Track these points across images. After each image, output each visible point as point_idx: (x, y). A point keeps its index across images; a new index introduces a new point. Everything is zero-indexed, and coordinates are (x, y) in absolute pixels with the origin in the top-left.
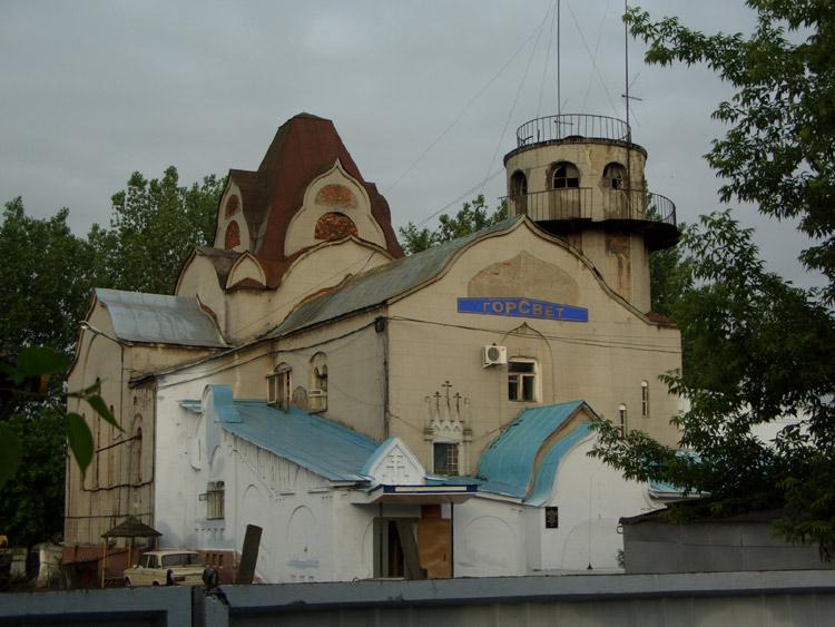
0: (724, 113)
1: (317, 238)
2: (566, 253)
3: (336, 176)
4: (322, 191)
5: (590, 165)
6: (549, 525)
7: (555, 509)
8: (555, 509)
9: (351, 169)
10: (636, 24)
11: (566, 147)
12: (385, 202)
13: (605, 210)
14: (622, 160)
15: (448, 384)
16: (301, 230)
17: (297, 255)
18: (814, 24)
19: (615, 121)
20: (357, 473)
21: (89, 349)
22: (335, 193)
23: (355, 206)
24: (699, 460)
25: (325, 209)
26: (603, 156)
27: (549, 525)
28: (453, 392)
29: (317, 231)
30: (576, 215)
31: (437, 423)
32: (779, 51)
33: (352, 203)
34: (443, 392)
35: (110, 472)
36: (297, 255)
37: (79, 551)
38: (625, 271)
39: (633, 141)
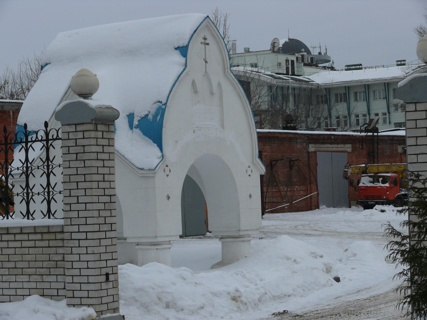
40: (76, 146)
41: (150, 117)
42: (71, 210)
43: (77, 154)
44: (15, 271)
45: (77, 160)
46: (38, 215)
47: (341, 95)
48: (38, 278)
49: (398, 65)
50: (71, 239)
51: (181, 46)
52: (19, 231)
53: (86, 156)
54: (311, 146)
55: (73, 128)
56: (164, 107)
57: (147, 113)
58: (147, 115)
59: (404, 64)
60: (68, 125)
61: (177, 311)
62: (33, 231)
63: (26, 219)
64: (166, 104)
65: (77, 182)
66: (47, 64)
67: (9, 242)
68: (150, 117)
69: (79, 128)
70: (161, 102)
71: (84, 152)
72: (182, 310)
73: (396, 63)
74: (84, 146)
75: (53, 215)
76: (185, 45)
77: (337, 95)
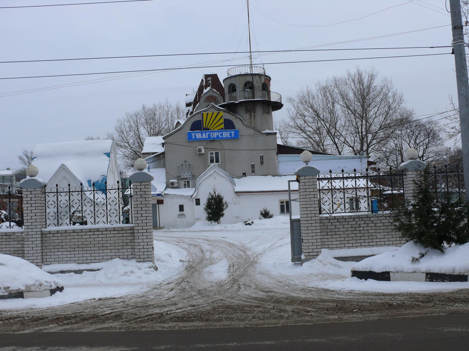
2: (229, 114)
4: (206, 98)
5: (258, 84)
6: (197, 204)
7: (199, 199)
8: (199, 199)
11: (232, 78)
14: (251, 80)
15: (185, 161)
18: (444, 241)
19: (261, 68)
21: (214, 126)
26: (243, 82)
27: (197, 204)
28: (187, 164)
31: (182, 173)
34: (184, 164)
37: (461, 29)
38: (253, 117)
39: (266, 74)
40: (141, 191)
41: (100, 182)
42: (138, 220)
43: (141, 195)
44: (102, 248)
45: (141, 198)
46: (113, 222)
47: (8, 179)
48: (117, 251)
49: (7, 170)
50: (138, 233)
51: (107, 152)
52: (105, 230)
53: (146, 196)
54: (4, 199)
55: (139, 184)
56: (106, 178)
57: (98, 180)
58: (98, 181)
59: (9, 170)
60: (136, 182)
61: (162, 262)
62: (113, 230)
63: (9, 229)
64: (107, 176)
65: (142, 208)
66: (35, 158)
67: (91, 236)
68: (100, 182)
69: (142, 184)
70: (104, 176)
71: (145, 194)
72: (164, 261)
73: (6, 169)
74: (145, 192)
75: (12, 227)
76: (109, 152)
77: (6, 179)
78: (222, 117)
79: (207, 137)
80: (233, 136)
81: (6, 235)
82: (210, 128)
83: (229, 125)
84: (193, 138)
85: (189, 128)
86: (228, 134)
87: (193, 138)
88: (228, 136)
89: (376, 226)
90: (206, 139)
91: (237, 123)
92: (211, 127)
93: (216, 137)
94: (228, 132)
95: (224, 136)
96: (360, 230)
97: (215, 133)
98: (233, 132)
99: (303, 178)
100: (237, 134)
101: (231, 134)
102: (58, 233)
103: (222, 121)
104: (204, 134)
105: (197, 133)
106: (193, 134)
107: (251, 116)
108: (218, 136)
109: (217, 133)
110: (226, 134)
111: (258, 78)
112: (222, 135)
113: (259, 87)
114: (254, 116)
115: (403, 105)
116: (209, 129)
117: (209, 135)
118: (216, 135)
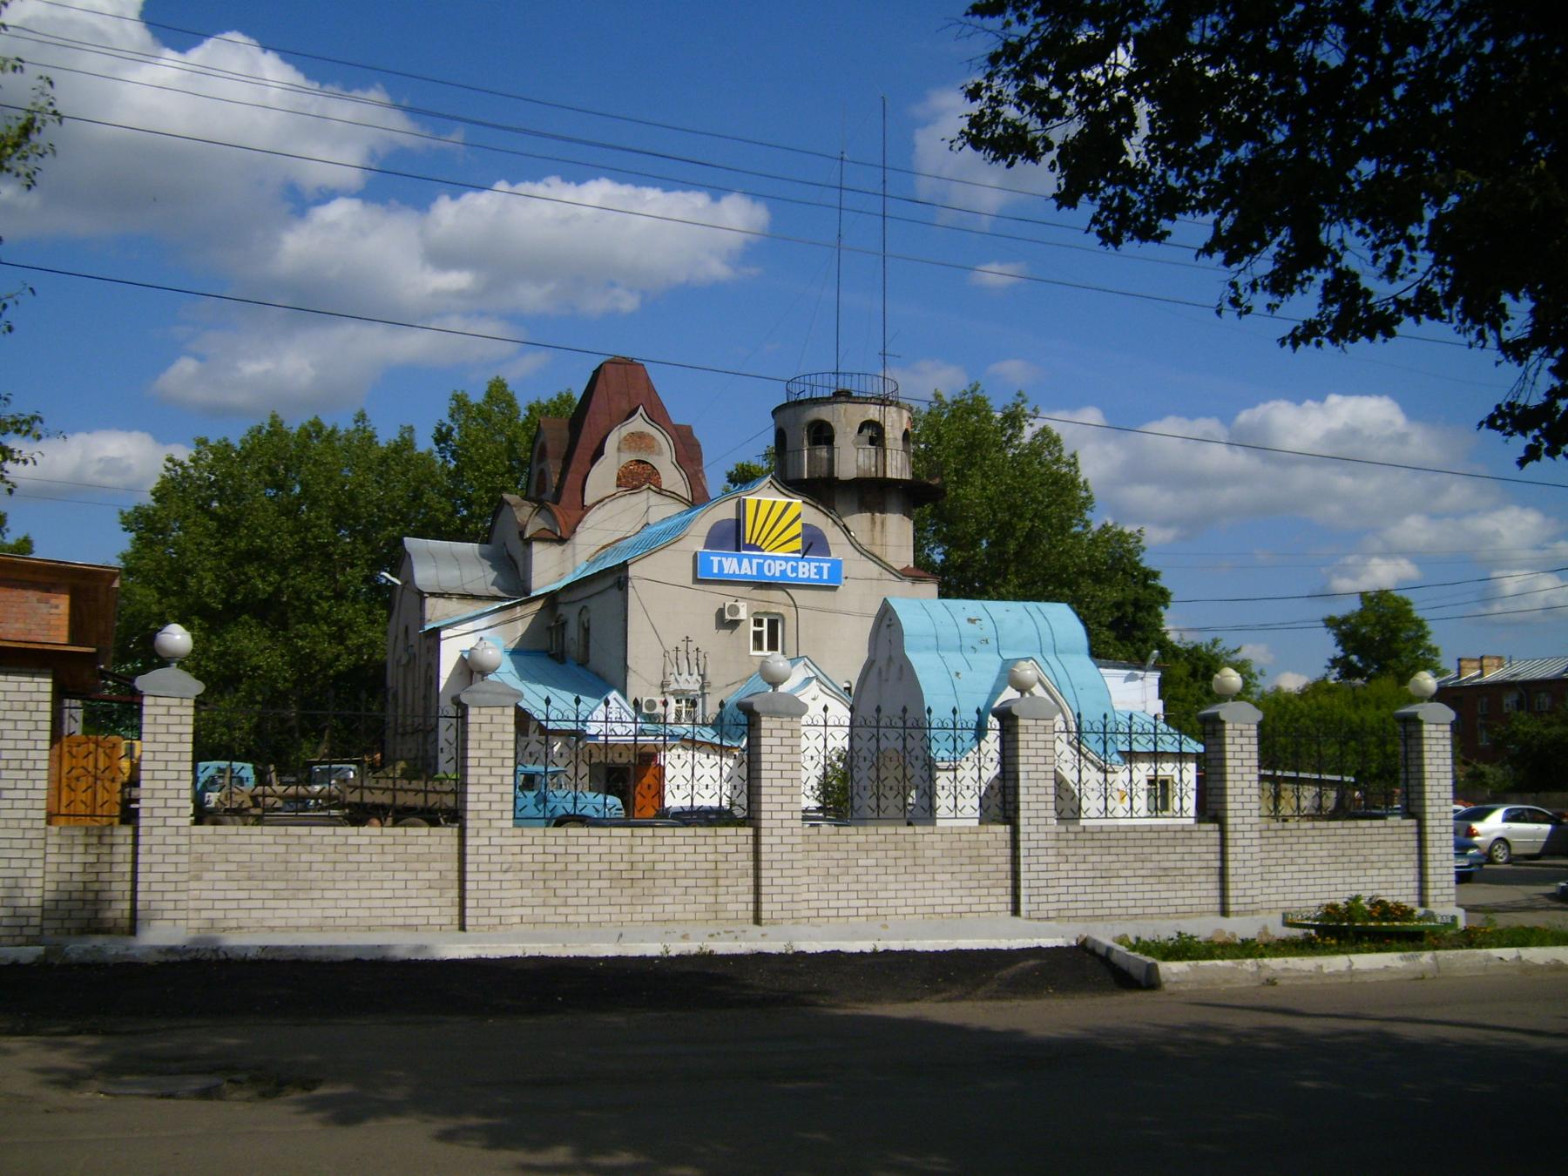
0: (1319, 344)
1: (618, 486)
3: (638, 424)
9: (657, 415)
10: (1282, 342)
12: (699, 446)
13: (858, 467)
16: (602, 478)
17: (594, 505)
20: (1355, 577)
22: (638, 439)
23: (660, 453)
24: (1285, 234)
25: (628, 457)
29: (619, 479)
30: (880, 475)
32: (1088, 191)
33: (656, 448)
35: (704, 714)
36: (594, 505)
48: (966, 892)
78: (799, 516)
79: (755, 573)
80: (825, 577)
81: (1183, 831)
82: (758, 544)
83: (813, 543)
84: (715, 571)
85: (703, 540)
86: (814, 570)
87: (715, 571)
88: (813, 576)
89: (545, 881)
90: (752, 576)
91: (833, 534)
92: (766, 543)
93: (778, 574)
94: (813, 564)
95: (800, 576)
96: (717, 878)
97: (778, 562)
98: (826, 566)
99: (1433, 727)
100: (836, 567)
101: (820, 570)
102: (1102, 832)
103: (797, 528)
104: (746, 562)
105: (727, 556)
106: (715, 560)
107: (873, 522)
108: (783, 572)
109: (784, 563)
110: (807, 570)
111: (894, 415)
112: (794, 569)
113: (896, 439)
114: (883, 524)
115: (523, 403)
116: (759, 549)
117: (760, 566)
118: (778, 568)
